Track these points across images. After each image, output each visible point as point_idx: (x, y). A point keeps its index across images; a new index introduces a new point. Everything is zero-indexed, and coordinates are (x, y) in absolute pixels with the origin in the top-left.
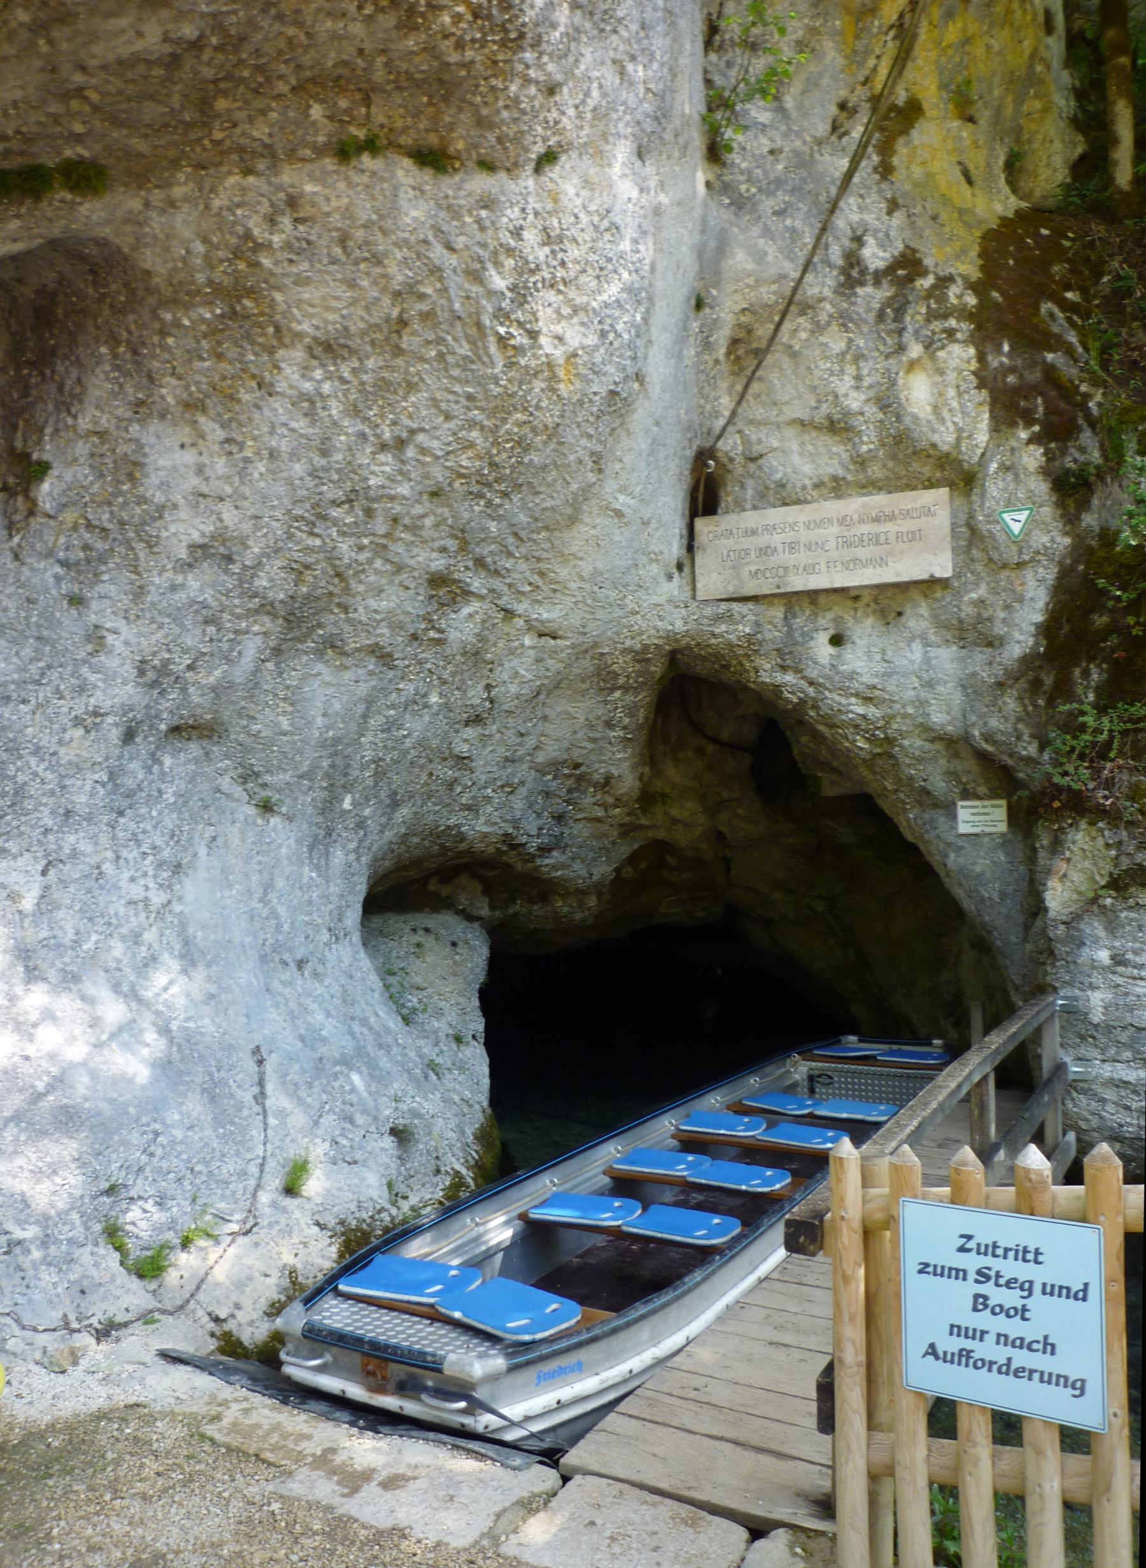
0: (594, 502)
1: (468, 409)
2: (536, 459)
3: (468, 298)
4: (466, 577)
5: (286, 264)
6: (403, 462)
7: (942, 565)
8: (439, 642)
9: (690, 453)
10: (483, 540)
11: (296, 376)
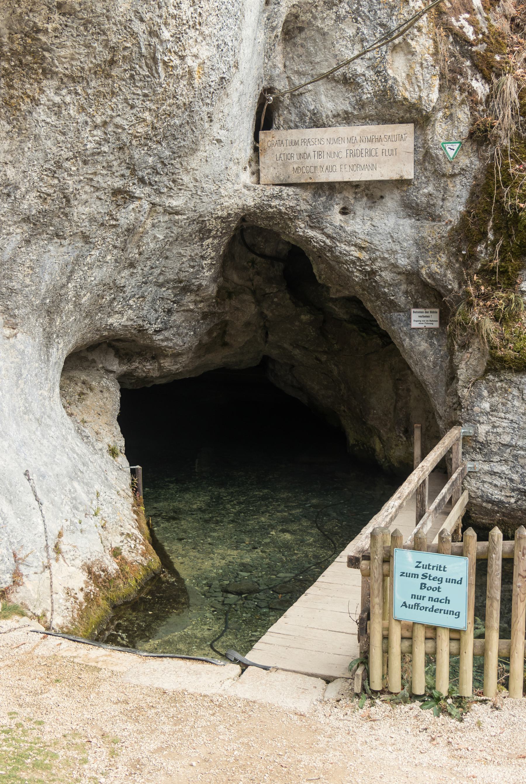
0: (206, 139)
1: (144, 101)
2: (177, 122)
3: (150, 45)
4: (132, 188)
6: (106, 133)
8: (114, 226)
9: (258, 92)
10: (145, 168)
11: (52, 94)
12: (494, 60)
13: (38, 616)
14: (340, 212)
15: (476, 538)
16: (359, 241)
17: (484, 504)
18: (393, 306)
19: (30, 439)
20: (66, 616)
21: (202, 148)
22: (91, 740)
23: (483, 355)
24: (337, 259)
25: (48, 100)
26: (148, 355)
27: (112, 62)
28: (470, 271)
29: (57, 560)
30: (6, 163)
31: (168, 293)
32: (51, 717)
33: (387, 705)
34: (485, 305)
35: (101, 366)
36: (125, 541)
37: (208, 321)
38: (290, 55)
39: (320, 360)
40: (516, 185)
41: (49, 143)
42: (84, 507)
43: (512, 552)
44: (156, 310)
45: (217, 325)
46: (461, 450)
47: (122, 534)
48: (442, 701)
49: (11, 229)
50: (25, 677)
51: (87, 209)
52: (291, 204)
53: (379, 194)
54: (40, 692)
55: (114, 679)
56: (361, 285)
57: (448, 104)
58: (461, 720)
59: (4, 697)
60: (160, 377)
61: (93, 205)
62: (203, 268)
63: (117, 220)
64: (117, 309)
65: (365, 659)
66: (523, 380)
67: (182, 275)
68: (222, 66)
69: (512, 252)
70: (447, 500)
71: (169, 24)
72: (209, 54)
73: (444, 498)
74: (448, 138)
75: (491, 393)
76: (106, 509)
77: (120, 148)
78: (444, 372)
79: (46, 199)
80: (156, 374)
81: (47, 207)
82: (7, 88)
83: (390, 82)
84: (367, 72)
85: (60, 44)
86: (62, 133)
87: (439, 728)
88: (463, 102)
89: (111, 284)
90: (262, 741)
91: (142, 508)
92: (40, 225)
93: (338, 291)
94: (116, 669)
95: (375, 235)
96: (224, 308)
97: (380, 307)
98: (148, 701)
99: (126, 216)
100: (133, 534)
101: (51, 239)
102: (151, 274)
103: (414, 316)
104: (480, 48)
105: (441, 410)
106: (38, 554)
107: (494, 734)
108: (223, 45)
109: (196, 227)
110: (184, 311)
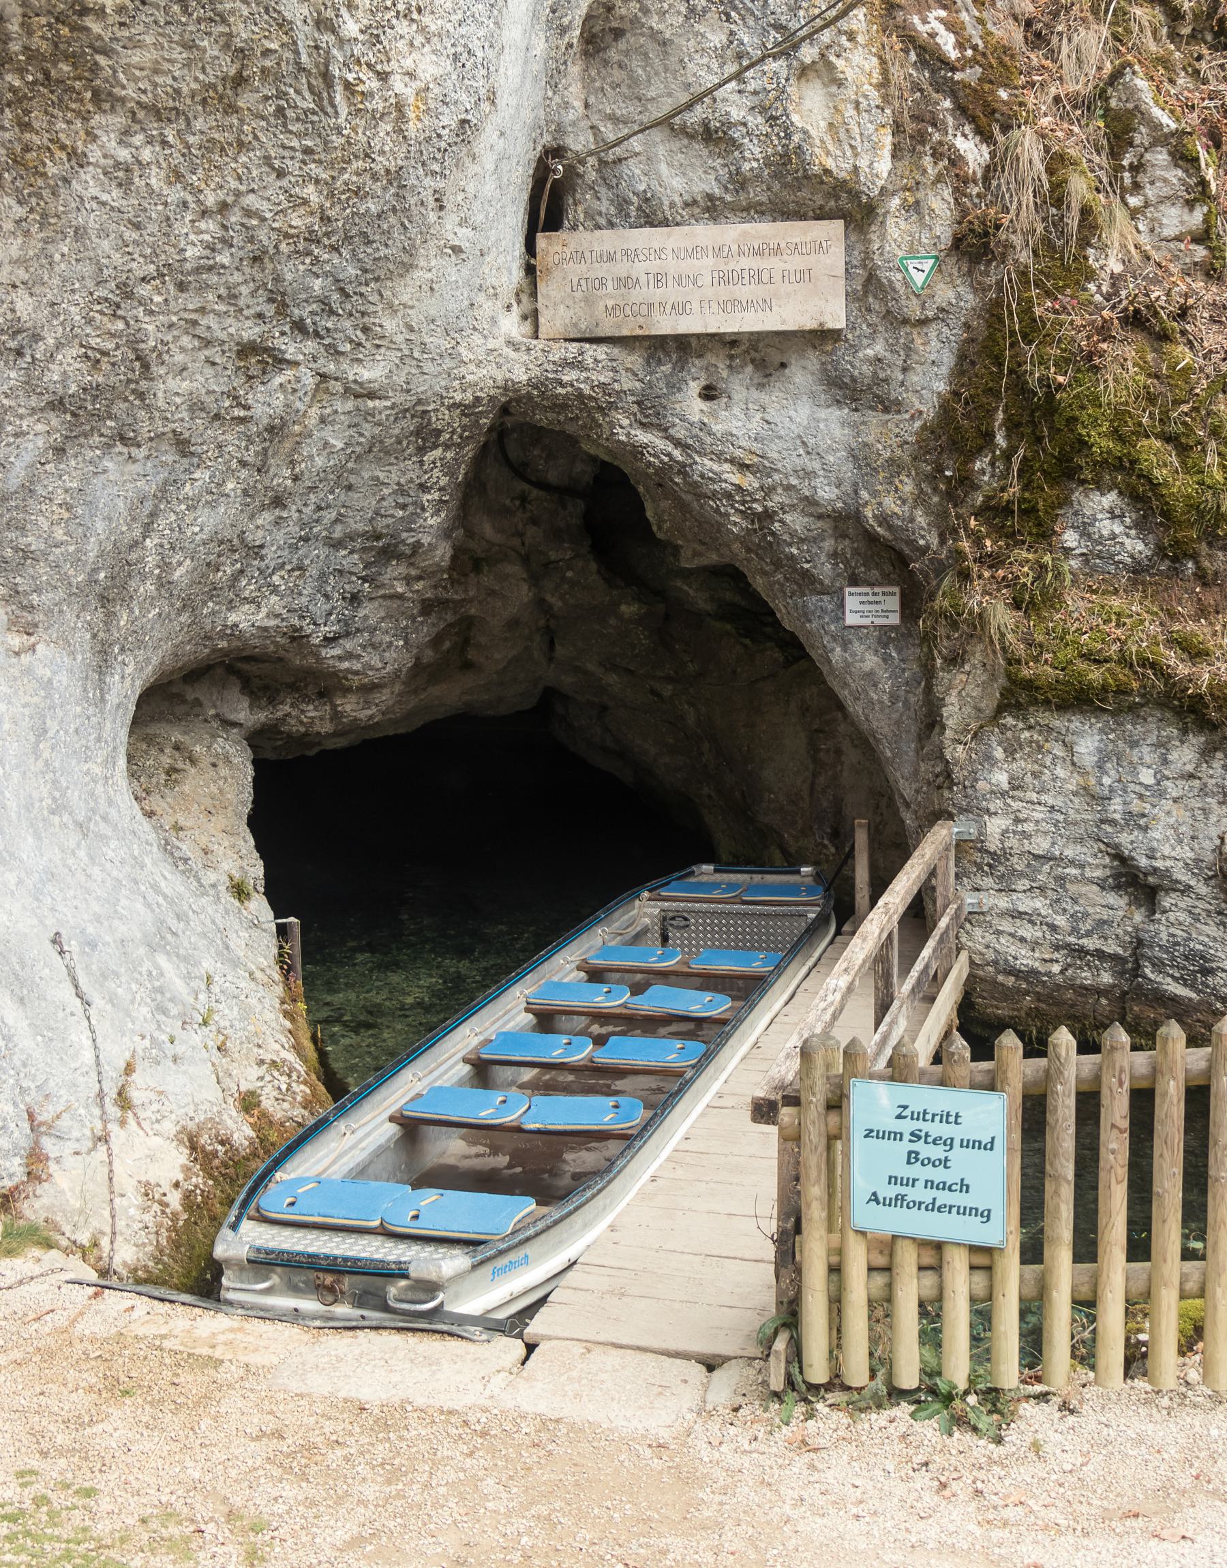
0: (431, 244)
1: (304, 162)
2: (373, 208)
3: (317, 47)
4: (279, 343)
5: (116, 28)
6: (225, 227)
7: (835, 315)
8: (242, 420)
10: (306, 301)
11: (114, 143)
12: (997, 99)
13: (82, 1247)
14: (700, 395)
15: (1021, 1052)
16: (738, 453)
17: (1000, 978)
18: (807, 581)
19: (65, 866)
20: (144, 1244)
21: (422, 263)
22: (203, 1527)
23: (993, 677)
24: (696, 490)
25: (105, 156)
26: (311, 690)
27: (239, 81)
28: (962, 511)
29: (123, 1123)
30: (14, 286)
31: (349, 560)
32: (111, 1477)
33: (841, 1414)
34: (993, 577)
35: (212, 712)
36: (268, 1078)
37: (432, 619)
38: (598, 84)
39: (659, 695)
40: (1048, 339)
41: (105, 244)
42: (180, 1007)
43: (1097, 1079)
44: (327, 597)
45: (451, 625)
46: (953, 870)
47: (262, 1062)
48: (957, 1401)
49: (25, 424)
50: (54, 1388)
51: (186, 385)
52: (602, 379)
53: (777, 359)
54: (87, 1419)
55: (251, 1382)
56: (743, 540)
57: (911, 183)
58: (999, 1441)
59: (8, 1436)
60: (335, 734)
61: (198, 377)
62: (423, 509)
63: (249, 408)
64: (246, 594)
65: (790, 1315)
66: (1072, 726)
67: (381, 523)
68: (464, 97)
69: (1044, 472)
70: (932, 973)
71: (357, 7)
72: (438, 72)
73: (927, 967)
74: (912, 246)
75: (1010, 752)
76: (227, 1011)
77: (255, 259)
78: (912, 713)
79: (98, 361)
80: (327, 728)
81: (101, 379)
82: (17, 129)
83: (796, 138)
84: (750, 118)
85: (130, 39)
86: (133, 224)
87: (953, 1462)
88: (939, 179)
89: (236, 541)
90: (579, 1509)
91: (302, 1006)
92: (91, 417)
93: (696, 554)
94: (255, 1359)
95: (771, 441)
96: (466, 591)
97: (782, 585)
98: (327, 1430)
99: (267, 400)
100: (284, 1061)
101: (109, 446)
102: (317, 521)
103: (851, 603)
104: (969, 76)
105: (907, 789)
106: (82, 1111)
107: (1068, 1467)
108: (465, 55)
109: (409, 424)
110: (384, 597)
